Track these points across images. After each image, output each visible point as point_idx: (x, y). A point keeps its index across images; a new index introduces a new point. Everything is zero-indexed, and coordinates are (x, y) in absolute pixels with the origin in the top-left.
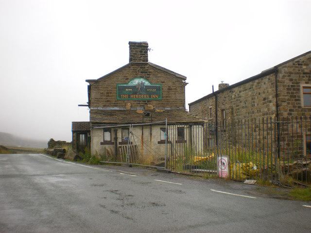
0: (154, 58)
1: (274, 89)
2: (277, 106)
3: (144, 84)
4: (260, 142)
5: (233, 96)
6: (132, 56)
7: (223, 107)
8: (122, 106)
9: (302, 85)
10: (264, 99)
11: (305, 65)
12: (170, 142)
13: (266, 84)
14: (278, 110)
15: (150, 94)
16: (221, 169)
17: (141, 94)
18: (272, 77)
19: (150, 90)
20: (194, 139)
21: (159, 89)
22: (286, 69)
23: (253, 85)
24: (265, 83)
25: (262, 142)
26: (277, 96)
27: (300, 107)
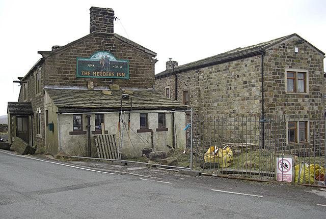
0: (119, 29)
1: (260, 71)
2: (263, 91)
3: (108, 61)
4: (237, 129)
5: (201, 77)
6: (95, 25)
7: (185, 88)
8: (83, 85)
9: (287, 69)
10: (245, 82)
11: (289, 48)
12: (151, 131)
13: (249, 67)
14: (264, 95)
15: (116, 71)
16: (283, 172)
17: (105, 71)
18: (257, 59)
19: (116, 67)
20: (177, 130)
21: (125, 65)
22: (272, 51)
23: (229, 66)
24: (246, 66)
25: (240, 128)
26: (262, 80)
27: (284, 93)
